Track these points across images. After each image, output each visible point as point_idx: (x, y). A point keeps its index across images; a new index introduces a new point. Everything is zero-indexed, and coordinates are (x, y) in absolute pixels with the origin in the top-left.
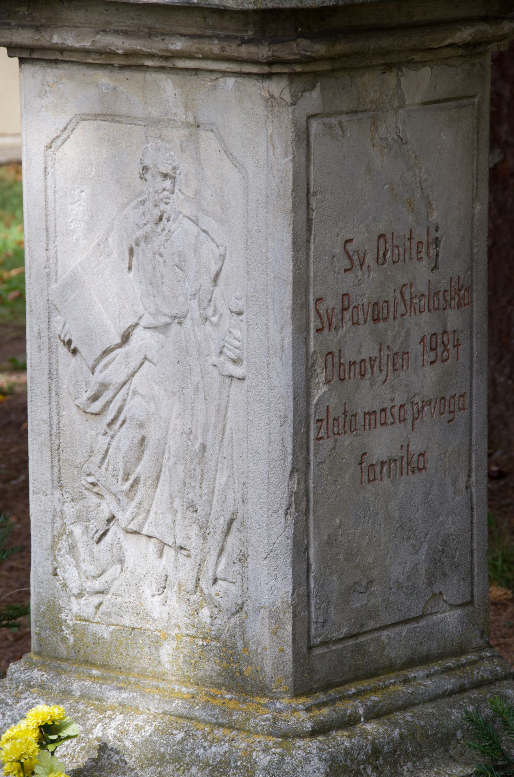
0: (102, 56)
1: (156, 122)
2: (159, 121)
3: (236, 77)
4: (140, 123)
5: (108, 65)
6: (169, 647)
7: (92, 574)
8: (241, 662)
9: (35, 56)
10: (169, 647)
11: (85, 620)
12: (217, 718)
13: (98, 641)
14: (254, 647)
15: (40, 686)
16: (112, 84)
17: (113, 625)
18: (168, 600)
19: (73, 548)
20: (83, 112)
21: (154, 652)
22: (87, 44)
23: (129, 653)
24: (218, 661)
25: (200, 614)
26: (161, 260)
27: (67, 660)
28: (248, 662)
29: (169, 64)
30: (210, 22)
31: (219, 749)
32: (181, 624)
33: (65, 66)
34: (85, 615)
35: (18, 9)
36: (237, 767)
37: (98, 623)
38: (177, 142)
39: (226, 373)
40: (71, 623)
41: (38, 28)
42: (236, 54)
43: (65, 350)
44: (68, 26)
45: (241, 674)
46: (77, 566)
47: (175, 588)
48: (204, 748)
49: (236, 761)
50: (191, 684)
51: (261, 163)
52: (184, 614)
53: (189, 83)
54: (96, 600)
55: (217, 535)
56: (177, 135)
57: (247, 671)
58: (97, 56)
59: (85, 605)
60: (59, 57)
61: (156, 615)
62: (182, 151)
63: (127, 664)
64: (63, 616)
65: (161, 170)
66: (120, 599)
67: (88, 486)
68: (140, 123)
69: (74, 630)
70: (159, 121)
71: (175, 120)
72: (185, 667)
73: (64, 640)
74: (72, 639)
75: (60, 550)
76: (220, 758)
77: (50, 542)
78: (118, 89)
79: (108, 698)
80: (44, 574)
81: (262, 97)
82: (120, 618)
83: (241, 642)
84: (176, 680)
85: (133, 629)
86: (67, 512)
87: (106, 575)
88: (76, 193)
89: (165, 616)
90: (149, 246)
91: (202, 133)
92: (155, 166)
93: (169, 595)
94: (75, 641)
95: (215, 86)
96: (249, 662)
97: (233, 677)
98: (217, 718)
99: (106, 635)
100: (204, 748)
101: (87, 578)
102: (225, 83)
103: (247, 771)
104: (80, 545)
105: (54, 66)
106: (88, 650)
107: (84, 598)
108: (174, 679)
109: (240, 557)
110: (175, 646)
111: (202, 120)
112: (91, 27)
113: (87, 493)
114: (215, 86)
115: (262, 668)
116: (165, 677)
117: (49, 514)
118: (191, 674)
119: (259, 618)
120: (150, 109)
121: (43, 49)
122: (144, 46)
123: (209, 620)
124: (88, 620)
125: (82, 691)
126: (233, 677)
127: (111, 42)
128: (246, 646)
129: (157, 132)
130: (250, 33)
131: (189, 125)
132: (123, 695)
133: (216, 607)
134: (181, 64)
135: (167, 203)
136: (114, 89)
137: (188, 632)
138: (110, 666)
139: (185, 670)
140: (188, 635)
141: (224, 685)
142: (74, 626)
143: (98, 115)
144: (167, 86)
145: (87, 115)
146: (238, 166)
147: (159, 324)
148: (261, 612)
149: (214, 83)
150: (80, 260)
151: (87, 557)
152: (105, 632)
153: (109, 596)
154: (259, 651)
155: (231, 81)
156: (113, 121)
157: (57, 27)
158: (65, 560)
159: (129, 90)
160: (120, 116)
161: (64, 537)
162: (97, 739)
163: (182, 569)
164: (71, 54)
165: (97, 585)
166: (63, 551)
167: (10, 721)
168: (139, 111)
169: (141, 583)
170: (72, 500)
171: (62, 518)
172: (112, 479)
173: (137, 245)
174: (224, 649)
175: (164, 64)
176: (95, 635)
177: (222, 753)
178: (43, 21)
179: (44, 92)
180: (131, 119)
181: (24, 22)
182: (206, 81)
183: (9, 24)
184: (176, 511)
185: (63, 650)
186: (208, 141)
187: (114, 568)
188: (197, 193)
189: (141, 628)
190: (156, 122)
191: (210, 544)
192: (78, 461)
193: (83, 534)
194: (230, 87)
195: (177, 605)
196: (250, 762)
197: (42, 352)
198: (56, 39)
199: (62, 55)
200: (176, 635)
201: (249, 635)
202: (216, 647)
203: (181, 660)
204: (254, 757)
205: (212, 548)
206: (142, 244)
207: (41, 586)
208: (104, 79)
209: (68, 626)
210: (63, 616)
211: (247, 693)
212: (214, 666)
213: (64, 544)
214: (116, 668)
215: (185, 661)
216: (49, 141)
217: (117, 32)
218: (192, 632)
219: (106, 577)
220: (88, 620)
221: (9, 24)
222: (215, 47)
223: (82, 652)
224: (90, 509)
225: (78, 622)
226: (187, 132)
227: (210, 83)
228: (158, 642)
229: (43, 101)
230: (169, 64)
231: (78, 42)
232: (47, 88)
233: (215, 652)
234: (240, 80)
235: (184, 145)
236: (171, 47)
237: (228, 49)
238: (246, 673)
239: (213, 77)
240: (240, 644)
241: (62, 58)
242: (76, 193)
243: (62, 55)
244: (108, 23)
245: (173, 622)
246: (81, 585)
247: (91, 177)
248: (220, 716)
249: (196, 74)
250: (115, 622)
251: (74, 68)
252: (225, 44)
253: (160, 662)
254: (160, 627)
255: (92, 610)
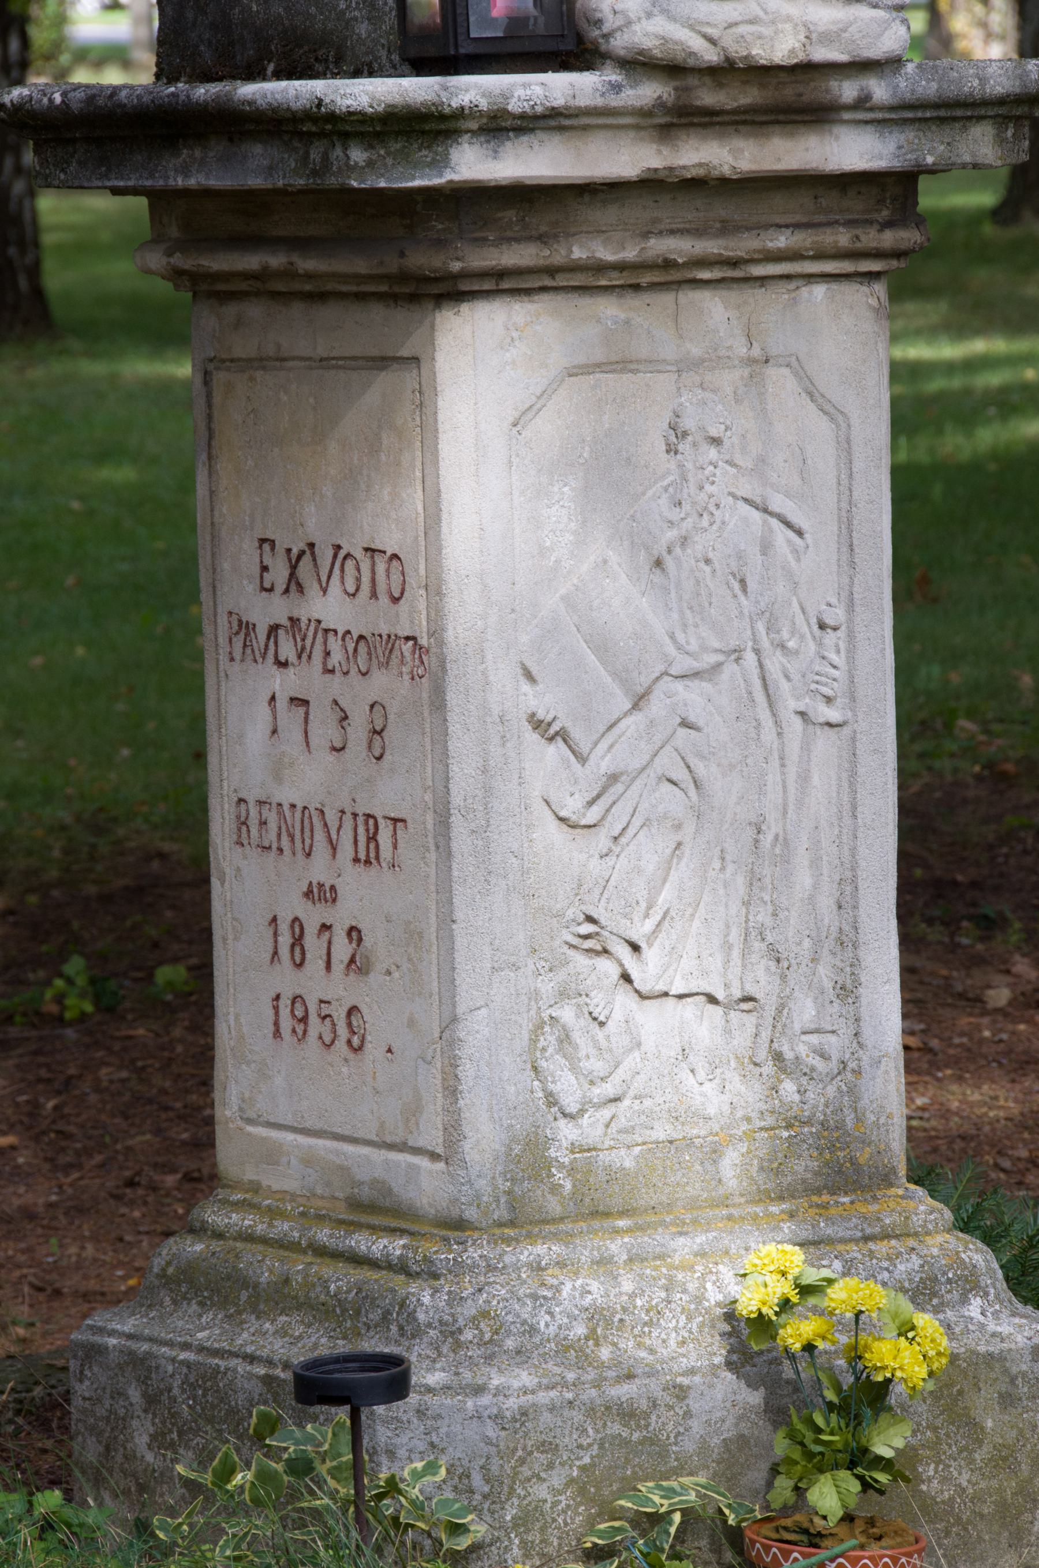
0: (624, 274)
1: (695, 364)
2: (703, 361)
3: (827, 282)
4: (669, 368)
5: (631, 286)
6: (736, 1154)
7: (602, 1075)
8: (852, 1146)
9: (505, 285)
10: (736, 1154)
11: (589, 1150)
12: (862, 1230)
13: (613, 1175)
14: (873, 1118)
15: (558, 1263)
16: (623, 316)
17: (637, 1145)
18: (727, 1084)
19: (565, 1038)
20: (576, 363)
21: (710, 1168)
22: (630, 254)
23: (668, 1181)
24: (815, 1154)
25: (782, 1092)
26: (708, 569)
27: (562, 1219)
28: (863, 1142)
29: (738, 273)
30: (824, 202)
31: (909, 1265)
32: (753, 1115)
33: (545, 297)
34: (590, 1141)
35: (500, 215)
36: (949, 1281)
37: (611, 1148)
38: (729, 390)
39: (822, 720)
40: (566, 1160)
41: (542, 239)
42: (874, 244)
43: (536, 736)
44: (587, 232)
45: (852, 1164)
46: (574, 1069)
47: (733, 1064)
48: (887, 1269)
49: (945, 1273)
50: (772, 1200)
51: (871, 402)
52: (757, 1097)
53: (751, 300)
54: (606, 1113)
55: (803, 966)
56: (729, 379)
57: (863, 1156)
58: (615, 274)
59: (590, 1125)
60: (548, 282)
61: (712, 1111)
62: (737, 401)
63: (664, 1198)
64: (552, 1153)
65: (711, 434)
66: (648, 1103)
67: (575, 941)
68: (669, 368)
69: (571, 1170)
70: (703, 361)
71: (729, 357)
72: (761, 1178)
73: (555, 1189)
74: (568, 1185)
75: (544, 1049)
76: (919, 1275)
77: (526, 1042)
78: (633, 322)
79: (675, 1251)
80: (519, 1094)
81: (870, 306)
82: (648, 1132)
83: (853, 1116)
84: (747, 1202)
85: (671, 1142)
86: (543, 990)
87: (620, 1070)
88: (556, 489)
89: (726, 1108)
90: (689, 551)
91: (772, 372)
92: (703, 429)
93: (728, 1075)
94: (574, 1186)
95: (794, 299)
96: (865, 1142)
97: (840, 1172)
98: (862, 1230)
99: (629, 1163)
100: (887, 1269)
101: (592, 1083)
102: (810, 293)
103: (967, 1280)
104: (576, 1036)
105: (526, 299)
106: (597, 1195)
107: (586, 1116)
108: (743, 1200)
109: (838, 991)
110: (744, 1150)
111: (773, 352)
112: (626, 230)
113: (571, 953)
114: (794, 299)
115: (887, 1145)
116: (729, 1202)
117: (524, 997)
118: (770, 1185)
119: (879, 1072)
120: (688, 345)
121: (551, 271)
122: (726, 248)
123: (797, 1097)
124: (595, 1149)
125: (629, 1252)
126: (840, 1172)
127: (673, 247)
128: (859, 1120)
129: (697, 379)
130: (885, 213)
131: (751, 361)
132: (698, 1240)
133: (805, 1074)
134: (758, 270)
135: (713, 483)
136: (627, 322)
137: (763, 1124)
138: (634, 1210)
139: (761, 1182)
140: (761, 1129)
141: (825, 1187)
142: (571, 1163)
143: (599, 365)
144: (715, 311)
145: (587, 366)
146: (830, 410)
147: (705, 666)
148: (883, 1063)
149: (793, 295)
150: (563, 591)
151: (592, 1051)
152: (626, 1160)
153: (627, 1102)
154: (882, 1121)
155: (819, 291)
156: (622, 371)
157: (568, 235)
158: (554, 1064)
159: (644, 321)
160: (638, 361)
161: (547, 1029)
162: (718, 1304)
163: (738, 1033)
164: (568, 275)
165: (609, 1089)
166: (550, 1050)
167: (566, 1320)
168: (669, 351)
169: (676, 1070)
170: (551, 970)
171: (537, 1001)
172: (624, 921)
173: (669, 552)
174: (826, 1133)
175: (730, 273)
176: (608, 1168)
177: (916, 1268)
178: (543, 228)
179: (509, 340)
180: (653, 364)
181: (509, 234)
182: (777, 296)
183: (485, 239)
184: (730, 947)
185: (554, 1206)
186: (781, 382)
187: (631, 1057)
188: (762, 460)
189: (684, 1138)
190: (695, 364)
191: (792, 983)
192: (558, 906)
193: (577, 1016)
194: (820, 297)
195: (743, 1088)
196: (966, 1268)
197: (509, 745)
198: (578, 253)
199: (554, 278)
200: (744, 1133)
201: (864, 1102)
202: (811, 1133)
203: (754, 1170)
204: (967, 1260)
205: (796, 988)
206: (678, 550)
207: (513, 1113)
208: (609, 310)
209: (561, 1166)
210: (552, 1153)
211: (863, 1188)
212: (809, 1163)
213: (549, 1038)
214: (646, 1210)
215: (762, 1168)
216: (516, 414)
217: (672, 232)
218: (770, 1121)
219: (621, 1074)
220: (595, 1149)
221: (485, 239)
222: (843, 238)
223: (587, 1200)
224: (581, 977)
225: (577, 1155)
226: (746, 372)
227: (786, 296)
228: (715, 1152)
229: (508, 355)
230: (738, 273)
231: (614, 253)
232: (515, 334)
233: (810, 1141)
234: (834, 286)
235: (740, 392)
236: (770, 245)
237: (863, 238)
238: (861, 1161)
239: (792, 285)
240: (850, 1120)
241: (555, 284)
242: (556, 489)
243: (554, 278)
244: (655, 221)
245: (739, 1114)
246: (584, 1097)
247: (582, 461)
248: (865, 1226)
249: (762, 286)
250: (640, 1140)
251: (559, 298)
252: (859, 232)
253: (720, 1181)
254: (716, 1128)
255: (600, 1130)
